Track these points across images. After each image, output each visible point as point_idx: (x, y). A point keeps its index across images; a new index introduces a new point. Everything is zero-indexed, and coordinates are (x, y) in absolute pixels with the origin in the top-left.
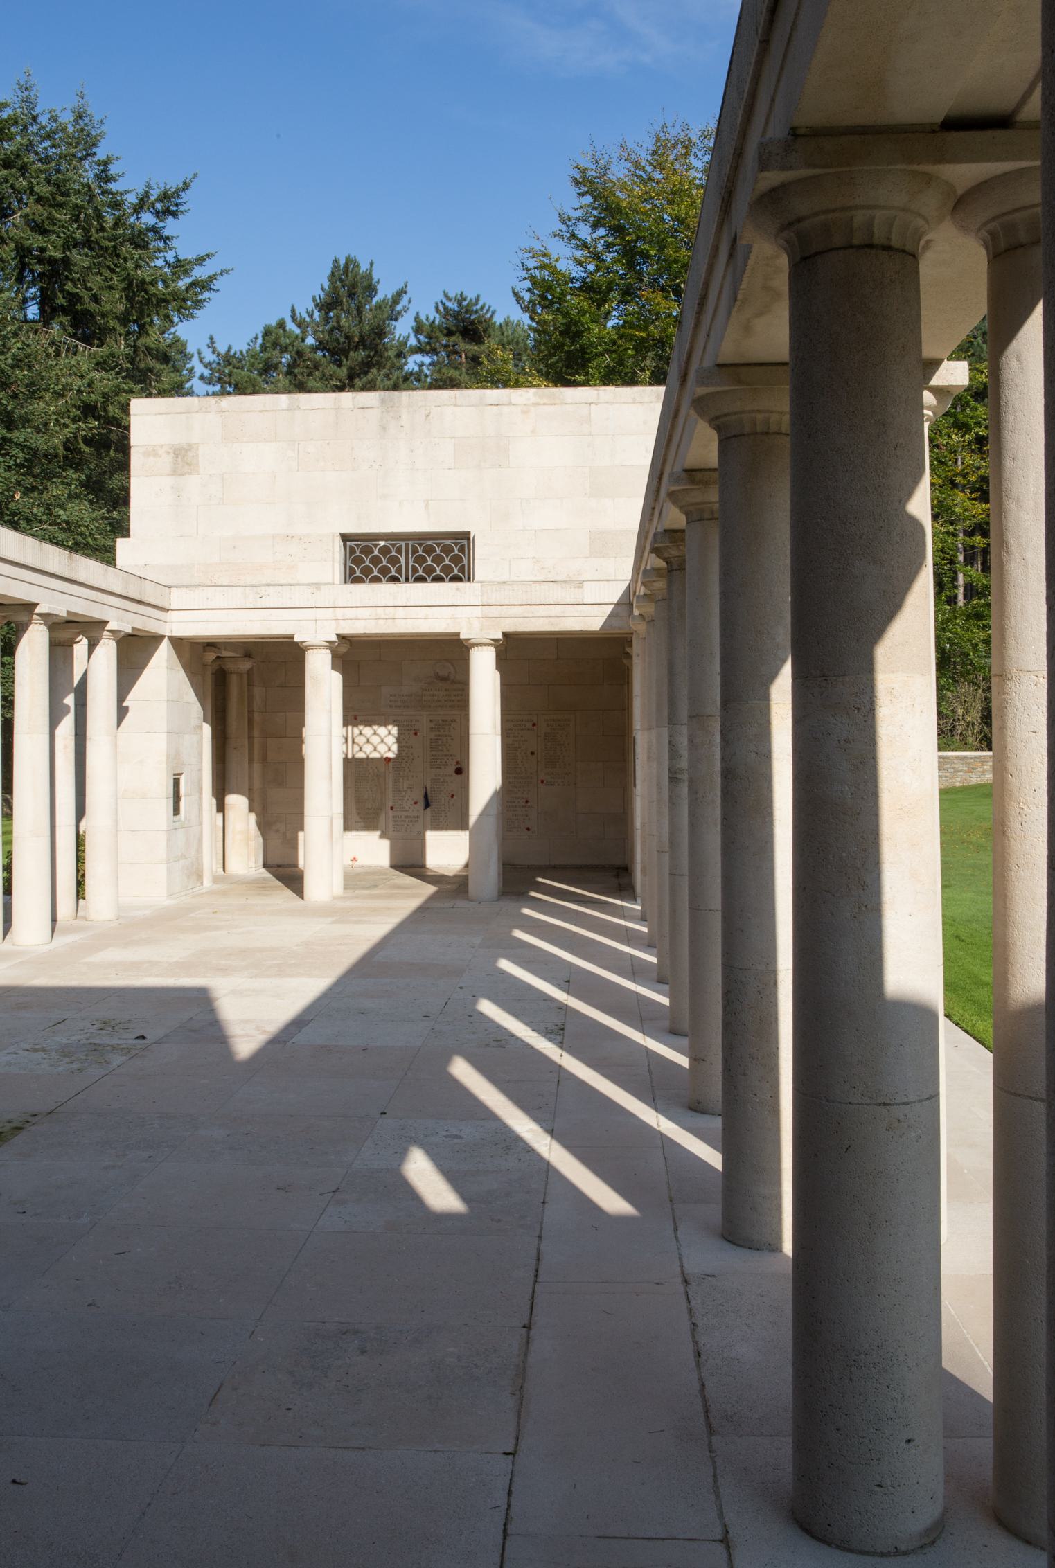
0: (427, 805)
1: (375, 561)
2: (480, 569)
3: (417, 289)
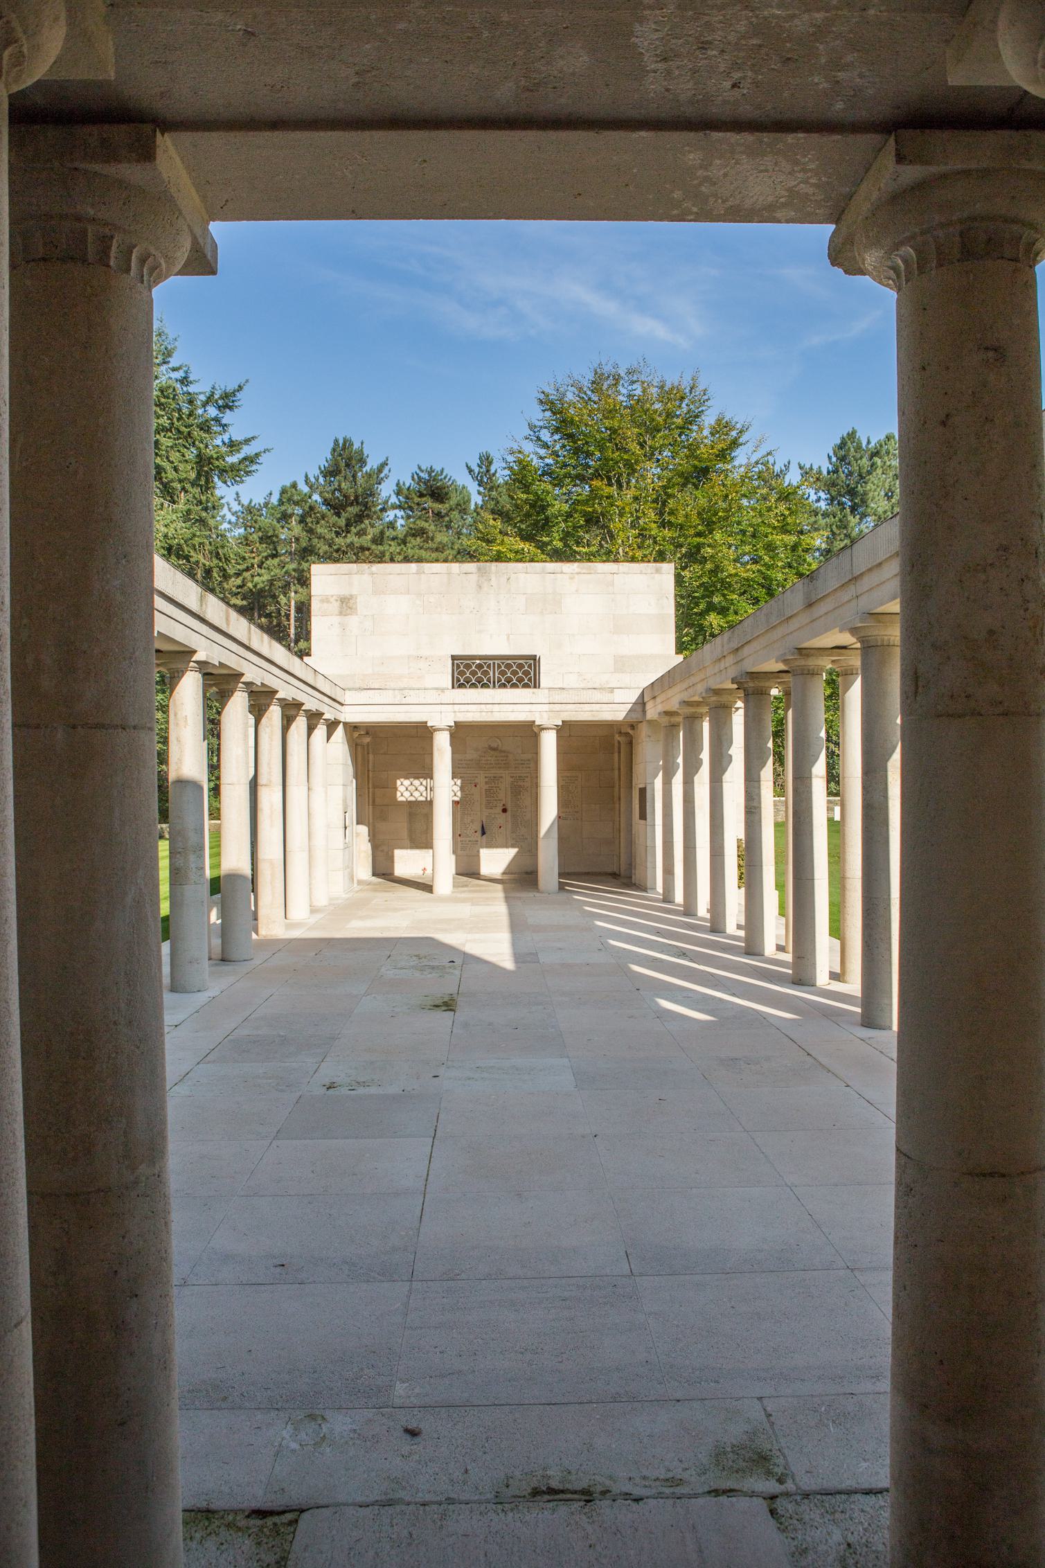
0: (483, 833)
1: (474, 673)
2: (544, 680)
3: (397, 463)
